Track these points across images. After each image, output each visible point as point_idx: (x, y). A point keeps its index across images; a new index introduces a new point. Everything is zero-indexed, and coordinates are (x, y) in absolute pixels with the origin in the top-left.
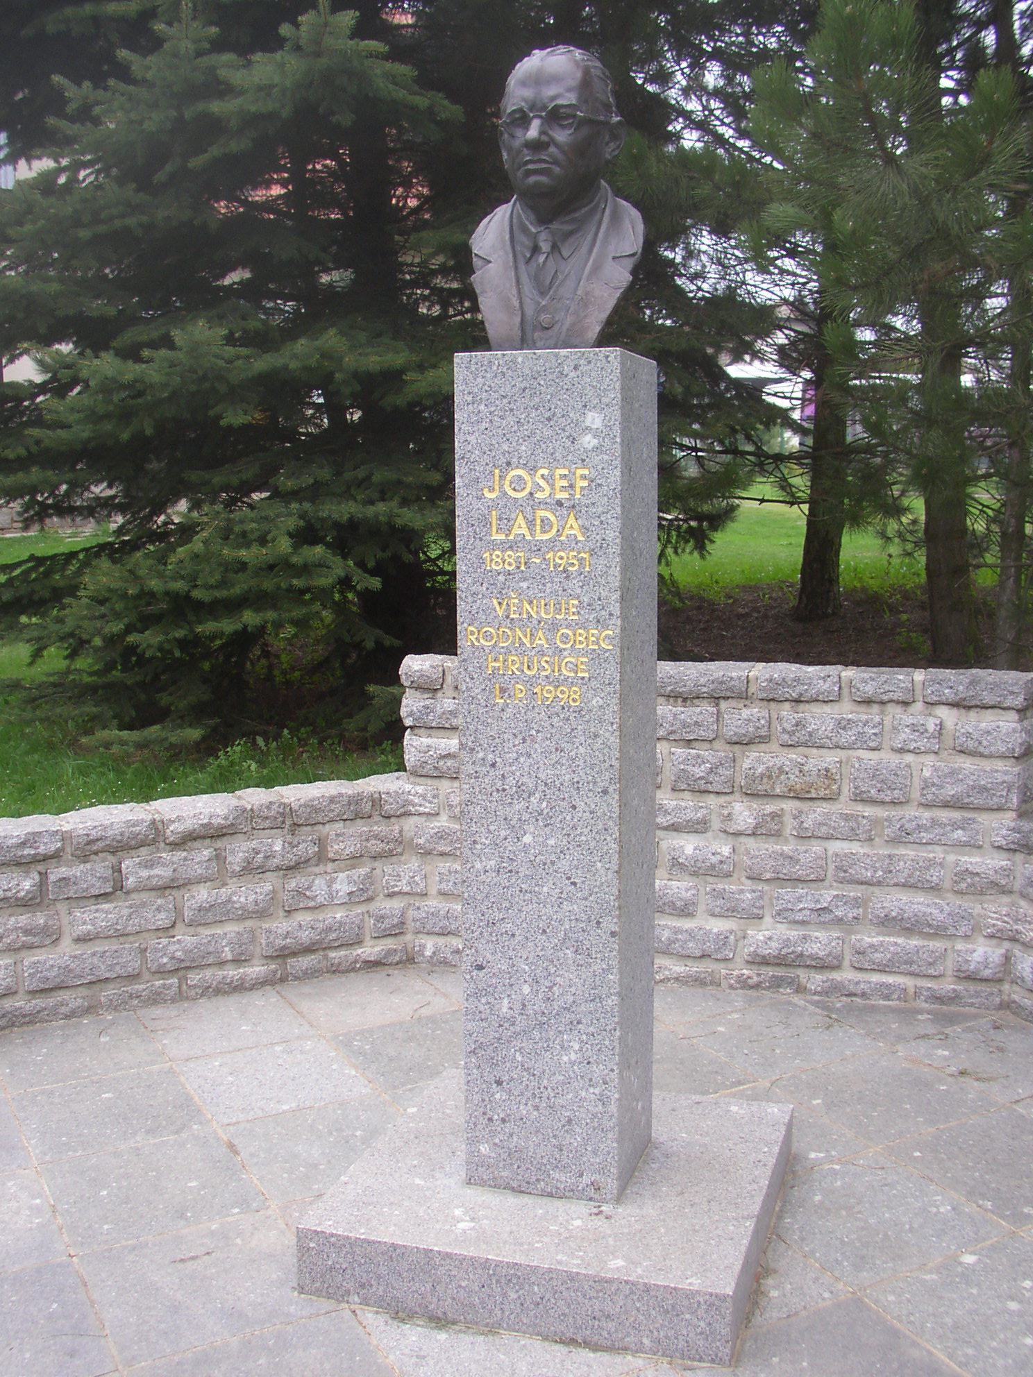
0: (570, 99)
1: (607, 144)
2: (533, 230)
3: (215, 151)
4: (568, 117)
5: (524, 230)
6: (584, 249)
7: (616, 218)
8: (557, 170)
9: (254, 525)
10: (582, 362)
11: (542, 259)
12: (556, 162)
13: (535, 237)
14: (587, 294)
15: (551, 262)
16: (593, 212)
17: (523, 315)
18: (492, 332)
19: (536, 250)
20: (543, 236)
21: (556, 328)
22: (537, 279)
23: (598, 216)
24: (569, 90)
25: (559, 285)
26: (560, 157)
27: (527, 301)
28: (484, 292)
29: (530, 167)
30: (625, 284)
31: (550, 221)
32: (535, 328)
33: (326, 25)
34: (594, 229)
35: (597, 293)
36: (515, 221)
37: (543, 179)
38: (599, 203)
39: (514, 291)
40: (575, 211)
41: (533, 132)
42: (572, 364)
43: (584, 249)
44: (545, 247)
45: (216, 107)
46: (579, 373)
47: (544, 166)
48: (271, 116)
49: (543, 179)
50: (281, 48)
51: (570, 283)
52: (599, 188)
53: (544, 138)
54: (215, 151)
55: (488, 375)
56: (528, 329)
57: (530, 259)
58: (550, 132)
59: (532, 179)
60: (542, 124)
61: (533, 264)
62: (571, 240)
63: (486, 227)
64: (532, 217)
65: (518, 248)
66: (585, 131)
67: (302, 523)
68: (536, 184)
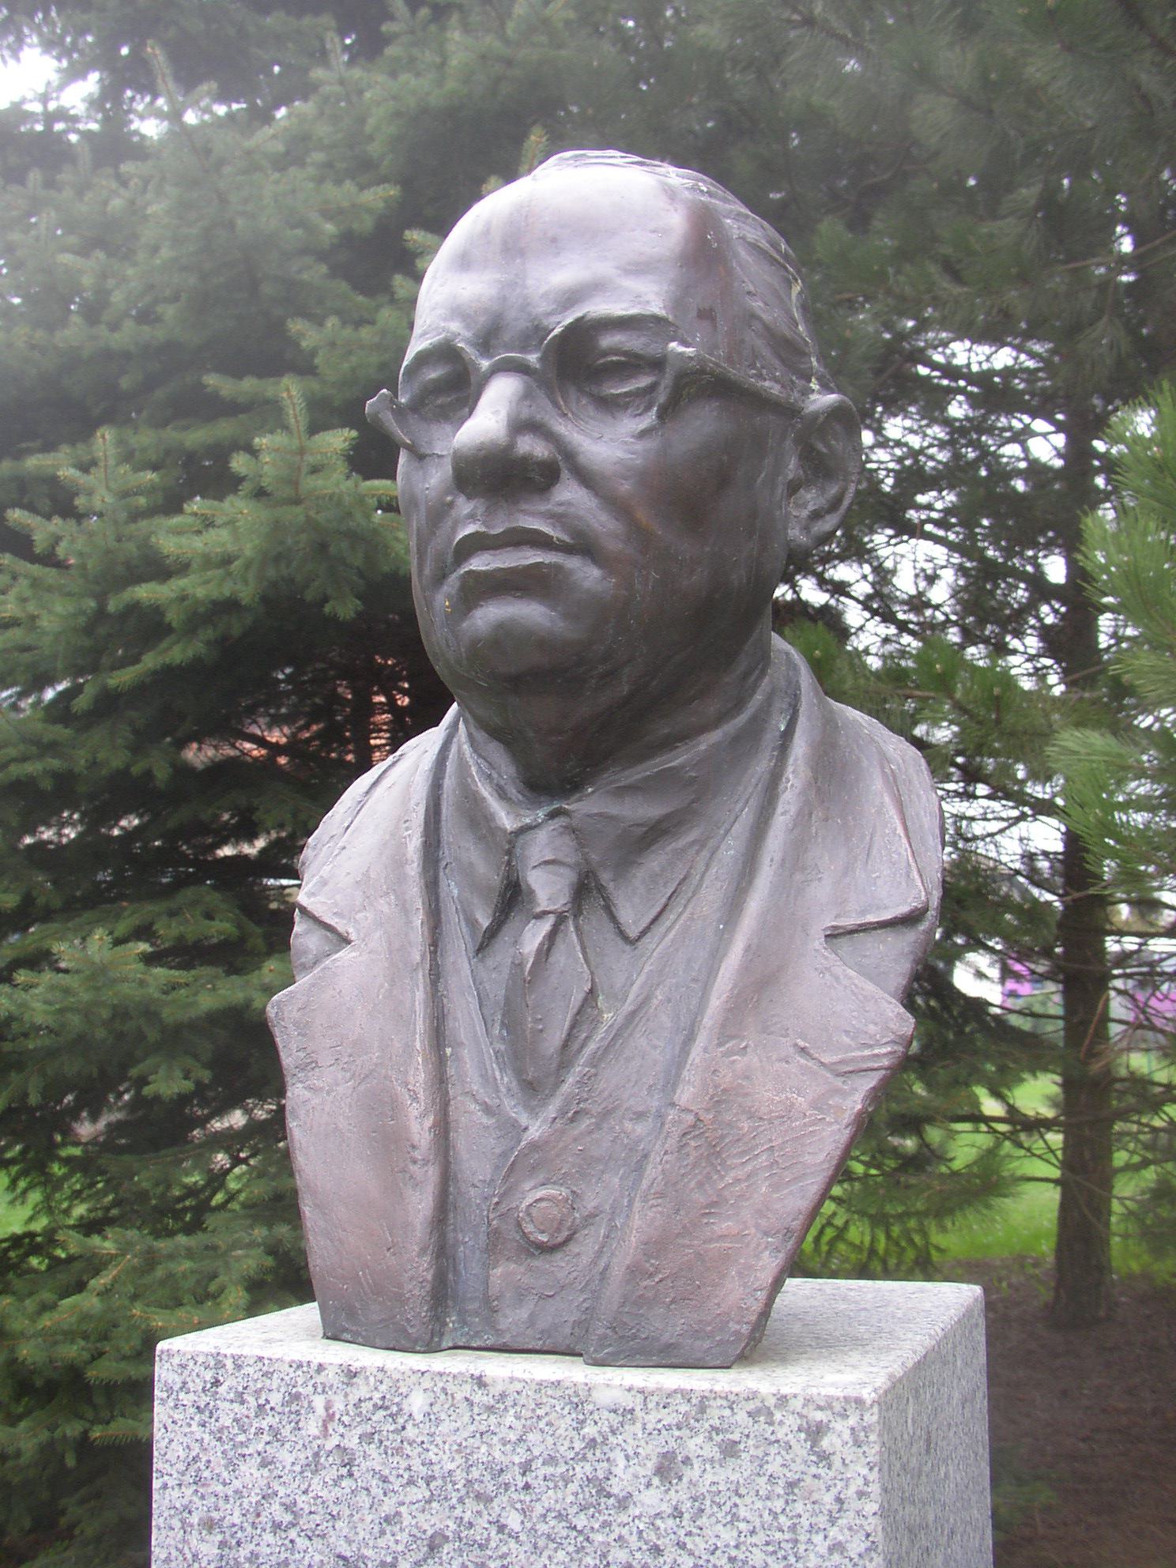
0: (649, 297)
1: (793, 488)
2: (506, 820)
3: (150, 661)
4: (632, 364)
5: (476, 818)
6: (711, 895)
7: (833, 772)
8: (588, 575)
9: (187, 1265)
10: (695, 1445)
11: (534, 936)
12: (583, 546)
13: (510, 846)
14: (720, 1099)
15: (568, 955)
16: (747, 740)
17: (447, 1178)
18: (327, 1239)
19: (512, 898)
20: (543, 844)
21: (586, 1247)
22: (513, 1020)
23: (761, 766)
24: (639, 268)
25: (595, 1061)
26: (601, 521)
27: (469, 1115)
28: (310, 1065)
29: (479, 563)
30: (884, 1053)
31: (571, 786)
32: (494, 1244)
33: (302, 451)
34: (747, 816)
35: (766, 1095)
36: (448, 783)
37: (530, 613)
38: (758, 724)
39: (419, 1076)
40: (668, 744)
41: (488, 419)
42: (652, 1450)
43: (711, 895)
44: (548, 889)
45: (144, 592)
46: (680, 1494)
47: (532, 557)
48: (230, 605)
49: (530, 613)
50: (235, 491)
51: (650, 1047)
52: (763, 658)
53: (531, 446)
54: (150, 661)
55: (285, 1456)
56: (468, 1243)
57: (492, 933)
58: (562, 428)
59: (490, 614)
60: (527, 395)
61: (501, 955)
62: (655, 861)
63: (361, 804)
64: (507, 769)
65: (451, 888)
66: (704, 423)
67: (269, 1261)
68: (504, 636)
